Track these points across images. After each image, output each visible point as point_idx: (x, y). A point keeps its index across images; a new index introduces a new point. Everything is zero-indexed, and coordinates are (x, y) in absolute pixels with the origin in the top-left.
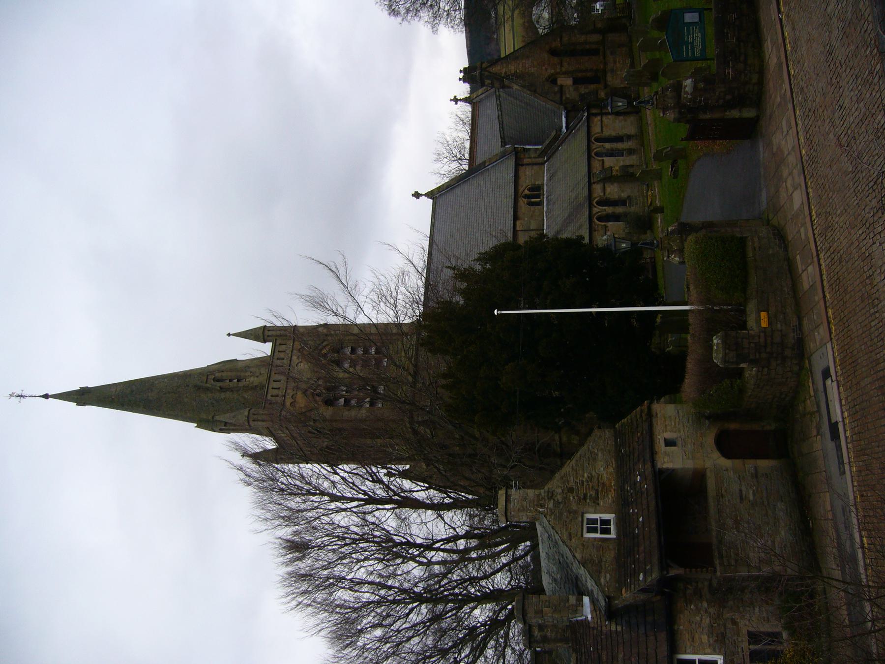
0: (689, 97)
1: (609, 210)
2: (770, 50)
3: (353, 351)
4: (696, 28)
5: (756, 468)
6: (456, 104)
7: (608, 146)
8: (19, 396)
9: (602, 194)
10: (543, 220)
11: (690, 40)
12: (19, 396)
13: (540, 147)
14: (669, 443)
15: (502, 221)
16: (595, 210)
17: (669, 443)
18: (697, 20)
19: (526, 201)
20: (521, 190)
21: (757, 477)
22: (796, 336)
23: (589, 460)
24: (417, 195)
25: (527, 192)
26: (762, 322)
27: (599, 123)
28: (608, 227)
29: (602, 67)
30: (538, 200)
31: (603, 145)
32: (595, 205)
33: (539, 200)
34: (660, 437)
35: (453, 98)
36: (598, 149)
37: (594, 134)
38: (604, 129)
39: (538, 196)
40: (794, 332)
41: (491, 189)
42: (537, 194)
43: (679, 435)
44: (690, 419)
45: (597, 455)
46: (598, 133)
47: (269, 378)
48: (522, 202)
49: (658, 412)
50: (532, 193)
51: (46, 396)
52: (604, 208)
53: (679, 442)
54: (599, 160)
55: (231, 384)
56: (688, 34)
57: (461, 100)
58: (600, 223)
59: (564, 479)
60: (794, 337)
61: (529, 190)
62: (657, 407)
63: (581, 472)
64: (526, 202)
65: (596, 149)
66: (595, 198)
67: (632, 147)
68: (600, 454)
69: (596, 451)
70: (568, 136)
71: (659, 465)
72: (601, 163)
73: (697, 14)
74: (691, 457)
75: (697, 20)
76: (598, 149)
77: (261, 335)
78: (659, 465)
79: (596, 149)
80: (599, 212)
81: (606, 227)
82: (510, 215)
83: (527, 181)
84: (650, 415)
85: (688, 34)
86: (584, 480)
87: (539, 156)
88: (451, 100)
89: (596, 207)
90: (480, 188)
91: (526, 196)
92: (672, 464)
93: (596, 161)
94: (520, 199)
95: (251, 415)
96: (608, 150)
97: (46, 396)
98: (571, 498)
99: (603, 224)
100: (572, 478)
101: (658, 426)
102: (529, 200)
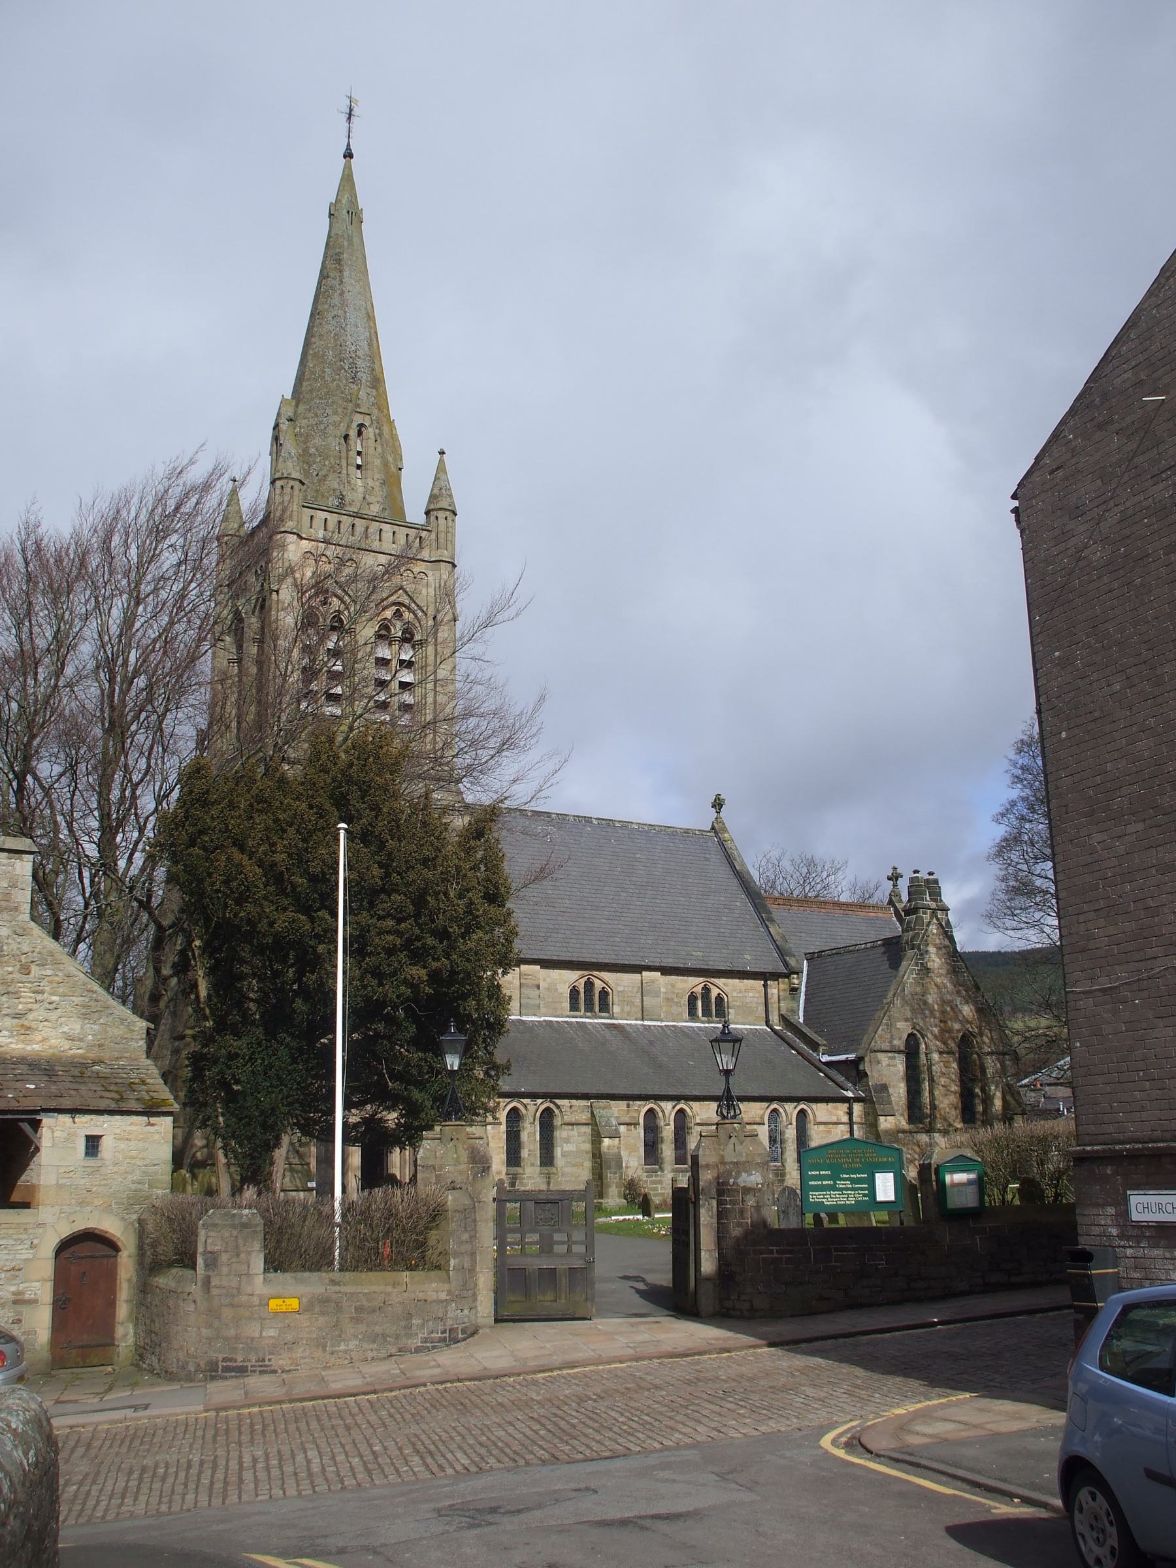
0: (731, 1181)
1: (668, 1131)
2: (950, 1426)
3: (409, 665)
4: (864, 1195)
5: (33, 1302)
6: (889, 879)
7: (791, 1133)
8: (351, 110)
9: (698, 1121)
10: (661, 1020)
11: (840, 1184)
12: (351, 110)
13: (801, 1020)
14: (93, 1144)
15: (661, 947)
16: (667, 1106)
17: (93, 1144)
18: (880, 1197)
19: (698, 990)
20: (720, 982)
21: (15, 1302)
22: (249, 1364)
23: (84, 1007)
24: (718, 804)
25: (715, 992)
26: (280, 1301)
27: (834, 1119)
28: (635, 1128)
29: (939, 1126)
30: (700, 1013)
31: (791, 1124)
32: (678, 1107)
33: (700, 1015)
34: (109, 1127)
35: (899, 871)
36: (784, 1114)
37: (812, 1110)
38: (822, 1127)
39: (707, 1012)
40: (258, 1361)
41: (722, 930)
42: (710, 1010)
43: (107, 1163)
44: (140, 1186)
45: (94, 1023)
46: (815, 1116)
47: (357, 516)
48: (694, 983)
49: (156, 1127)
50: (713, 1000)
51: (348, 155)
52: (672, 1123)
53: (91, 1162)
54: (763, 1115)
55: (353, 453)
56: (853, 1181)
57: (895, 886)
58: (642, 1114)
59: (49, 959)
60: (249, 1361)
61: (719, 999)
62: (165, 1124)
63: (61, 990)
64: (694, 990)
65: (785, 1111)
66: (691, 1108)
67: (788, 1177)
68: (96, 1027)
69: (102, 1021)
70: (813, 1064)
71: (47, 1121)
72: (758, 1120)
73: (893, 1198)
74: (61, 1181)
75: (880, 1197)
76: (784, 1114)
77: (439, 506)
78: (47, 1121)
79: (785, 1111)
80: (663, 1112)
81: (636, 1124)
82: (671, 960)
83: (735, 994)
84: (151, 1110)
85: (853, 1181)
86: (46, 995)
87: (782, 1017)
88: (895, 869)
89: (674, 1108)
90: (727, 911)
91: (706, 991)
92: (49, 1145)
93: (762, 1112)
94: (702, 979)
95: (292, 483)
96: (782, 1133)
97: (348, 155)
98: (10, 969)
99: (641, 1121)
100: (49, 972)
101: (134, 1124)
102: (699, 997)
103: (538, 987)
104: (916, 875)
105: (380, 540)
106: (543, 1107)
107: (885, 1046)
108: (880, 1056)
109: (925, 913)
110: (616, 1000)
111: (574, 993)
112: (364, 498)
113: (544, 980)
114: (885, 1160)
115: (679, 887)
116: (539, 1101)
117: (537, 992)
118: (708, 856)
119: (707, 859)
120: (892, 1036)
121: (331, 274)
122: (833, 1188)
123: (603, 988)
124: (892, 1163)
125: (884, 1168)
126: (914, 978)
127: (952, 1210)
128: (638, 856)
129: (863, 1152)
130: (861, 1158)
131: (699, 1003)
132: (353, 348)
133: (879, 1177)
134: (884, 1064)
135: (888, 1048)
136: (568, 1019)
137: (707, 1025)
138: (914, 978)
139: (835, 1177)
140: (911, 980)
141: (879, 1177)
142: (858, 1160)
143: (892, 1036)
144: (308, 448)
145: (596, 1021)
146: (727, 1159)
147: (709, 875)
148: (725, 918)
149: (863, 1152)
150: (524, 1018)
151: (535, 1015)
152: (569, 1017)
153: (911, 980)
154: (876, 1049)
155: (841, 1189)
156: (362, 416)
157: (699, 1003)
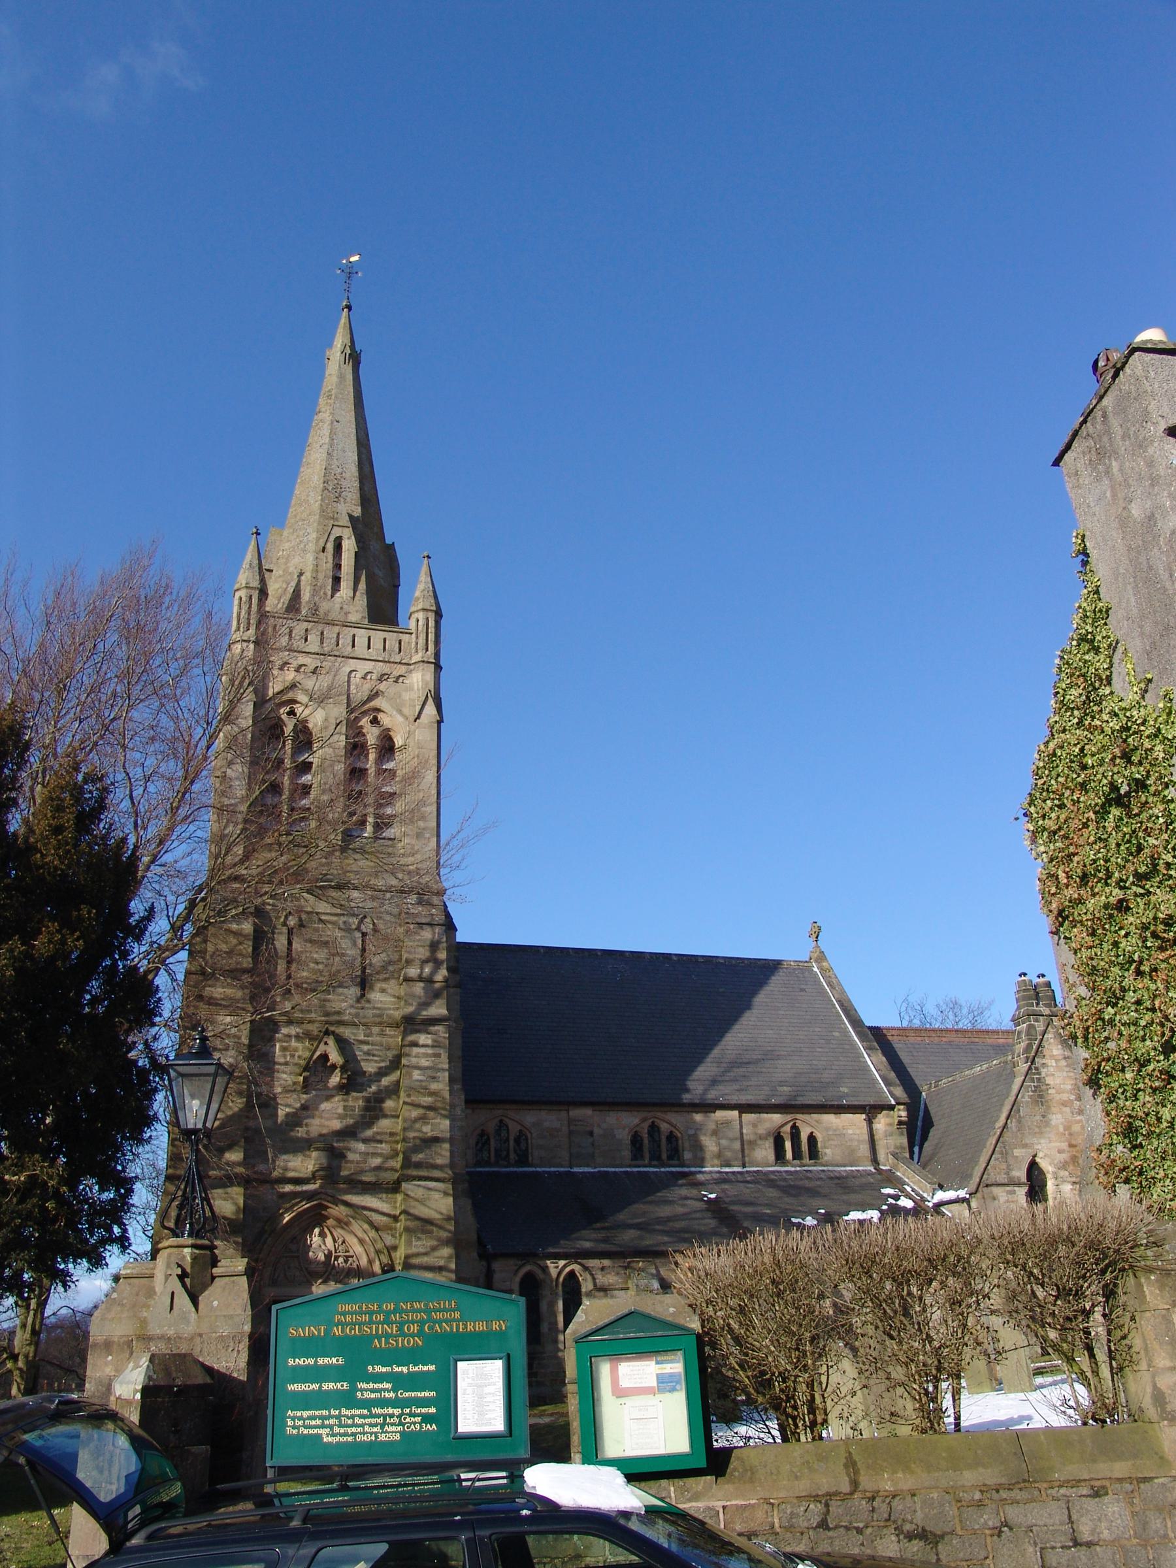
4: (427, 1419)
11: (366, 1390)
56: (399, 1382)
85: (399, 1382)
90: (823, 1041)
103: (591, 1134)
104: (1023, 978)
105: (353, 646)
106: (568, 1269)
107: (1002, 1178)
108: (996, 1191)
109: (1037, 1021)
110: (687, 1145)
111: (636, 1140)
112: (341, 608)
113: (599, 1126)
114: (481, 1326)
115: (767, 1019)
116: (562, 1263)
117: (590, 1140)
118: (803, 986)
119: (802, 990)
120: (1008, 1166)
121: (323, 410)
122: (348, 1399)
123: (671, 1132)
124: (501, 1334)
125: (478, 1349)
126: (1030, 1097)
127: (692, 1446)
128: (721, 990)
129: (427, 1311)
130: (422, 1323)
131: (788, 1145)
132: (339, 470)
133: (467, 1371)
134: (1002, 1200)
135: (1006, 1181)
136: (628, 1169)
137: (798, 1169)
138: (1030, 1097)
139: (354, 1372)
140: (1027, 1099)
141: (467, 1371)
142: (415, 1328)
143: (1008, 1166)
144: (288, 568)
145: (662, 1169)
146: (155, 1330)
147: (804, 1006)
148: (820, 1050)
149: (427, 1311)
150: (576, 1170)
151: (588, 1166)
152: (630, 1166)
153: (1027, 1099)
154: (989, 1182)
155: (368, 1404)
156: (340, 529)
157: (788, 1145)
